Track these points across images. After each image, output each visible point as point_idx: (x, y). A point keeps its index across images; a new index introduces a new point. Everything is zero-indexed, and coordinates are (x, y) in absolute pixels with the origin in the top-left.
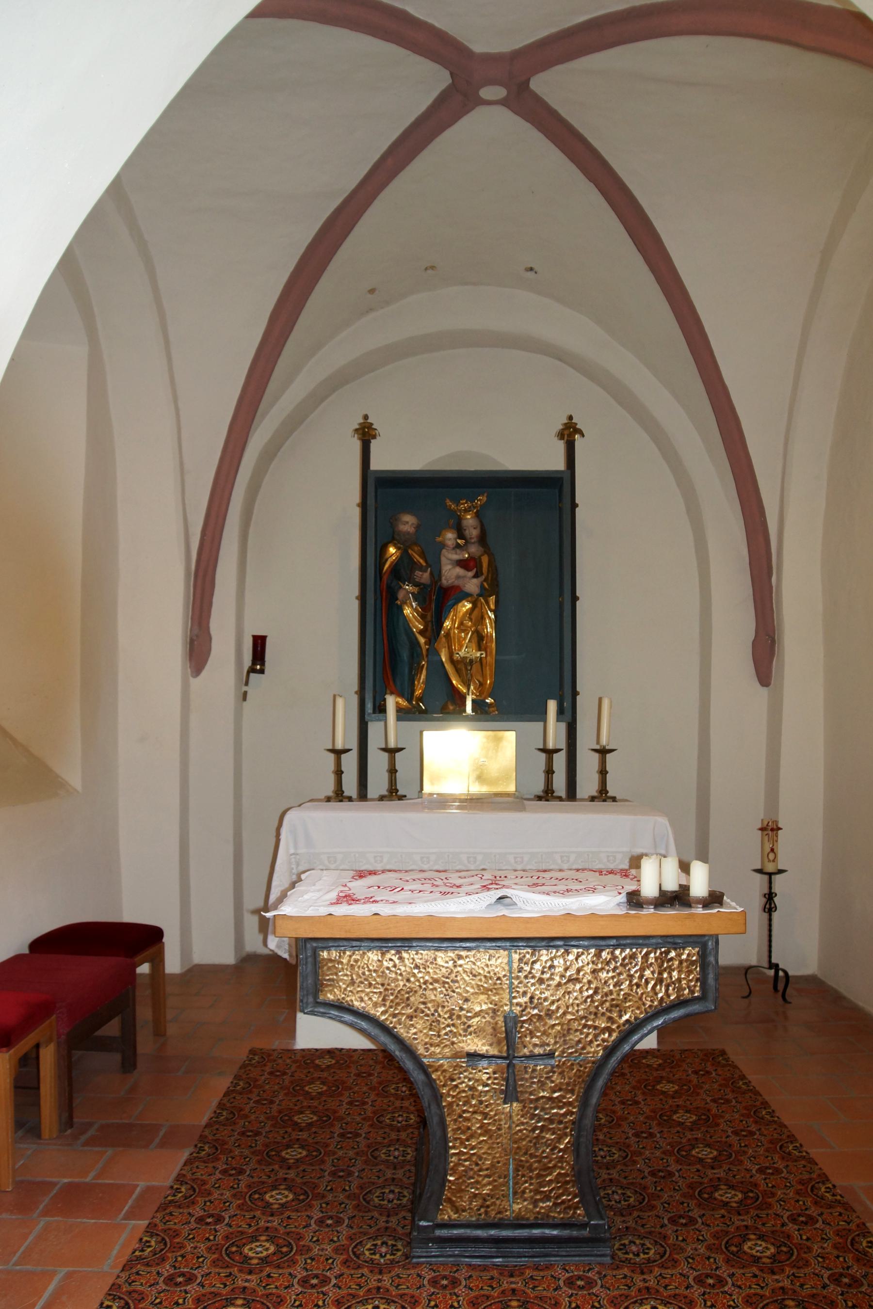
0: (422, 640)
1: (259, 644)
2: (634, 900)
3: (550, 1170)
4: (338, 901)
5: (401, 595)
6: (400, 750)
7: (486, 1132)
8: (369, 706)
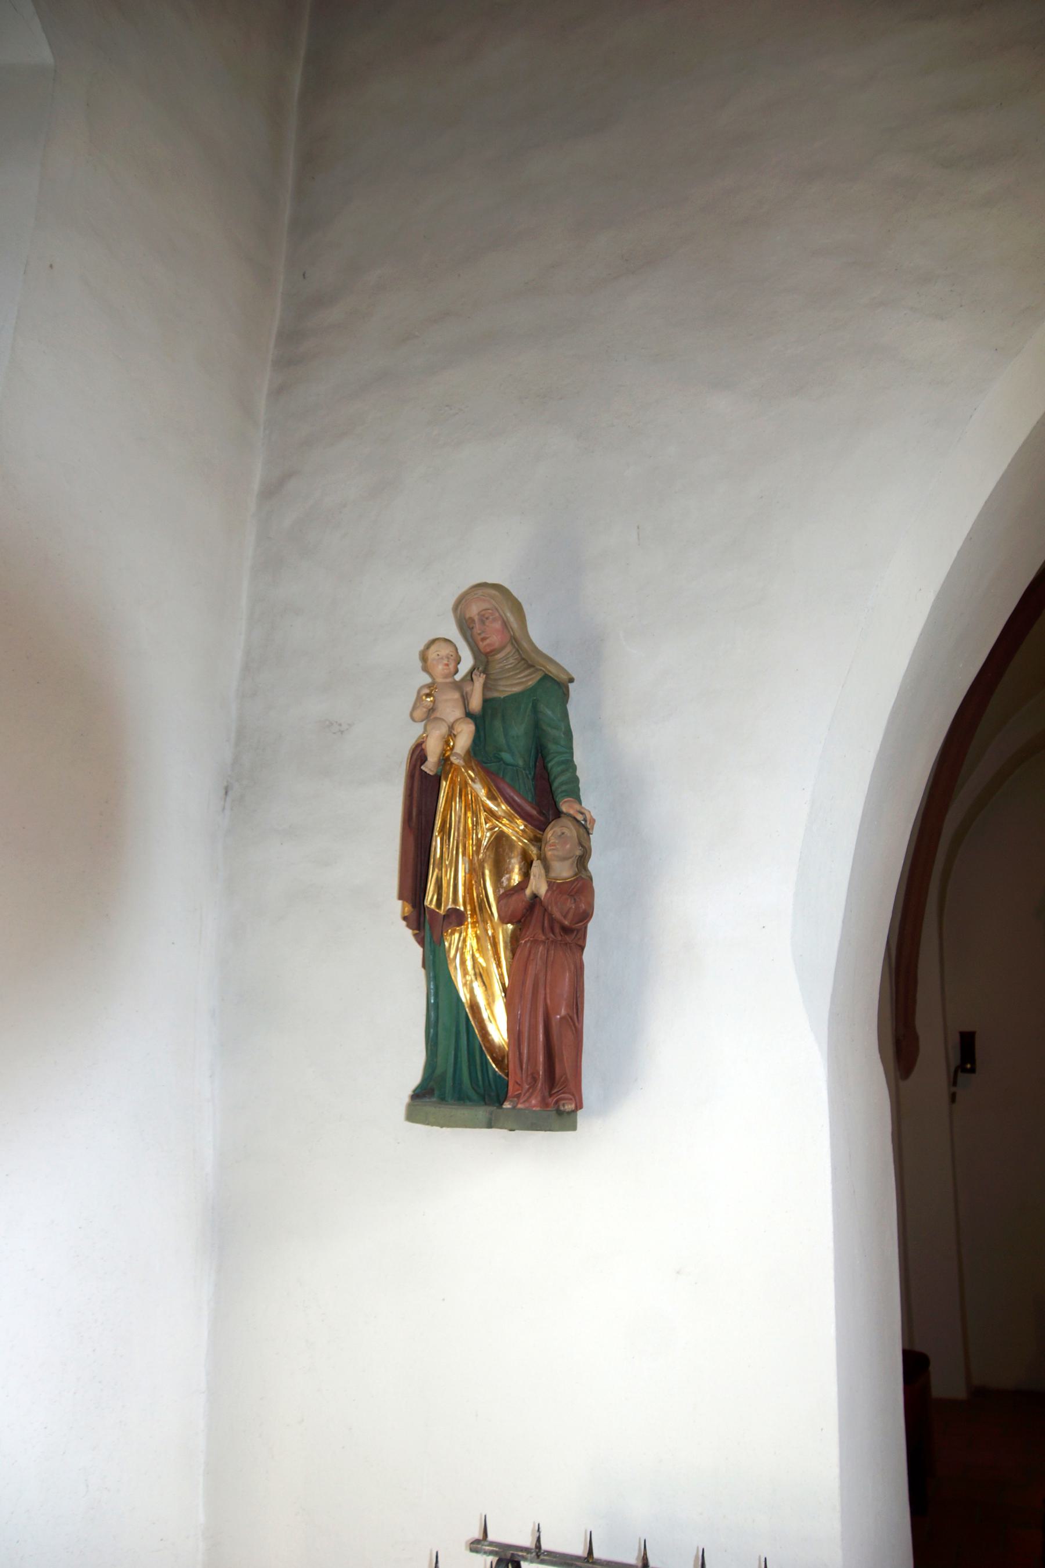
1: (967, 1042)
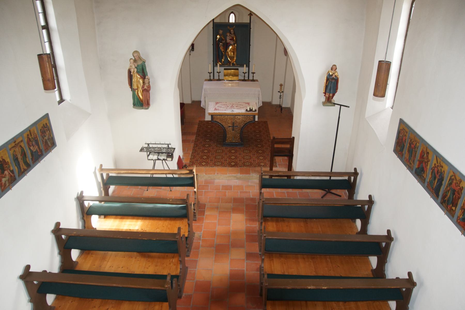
0: (223, 53)
2: (247, 110)
3: (237, 138)
5: (220, 45)
6: (220, 72)
7: (231, 134)
8: (215, 64)
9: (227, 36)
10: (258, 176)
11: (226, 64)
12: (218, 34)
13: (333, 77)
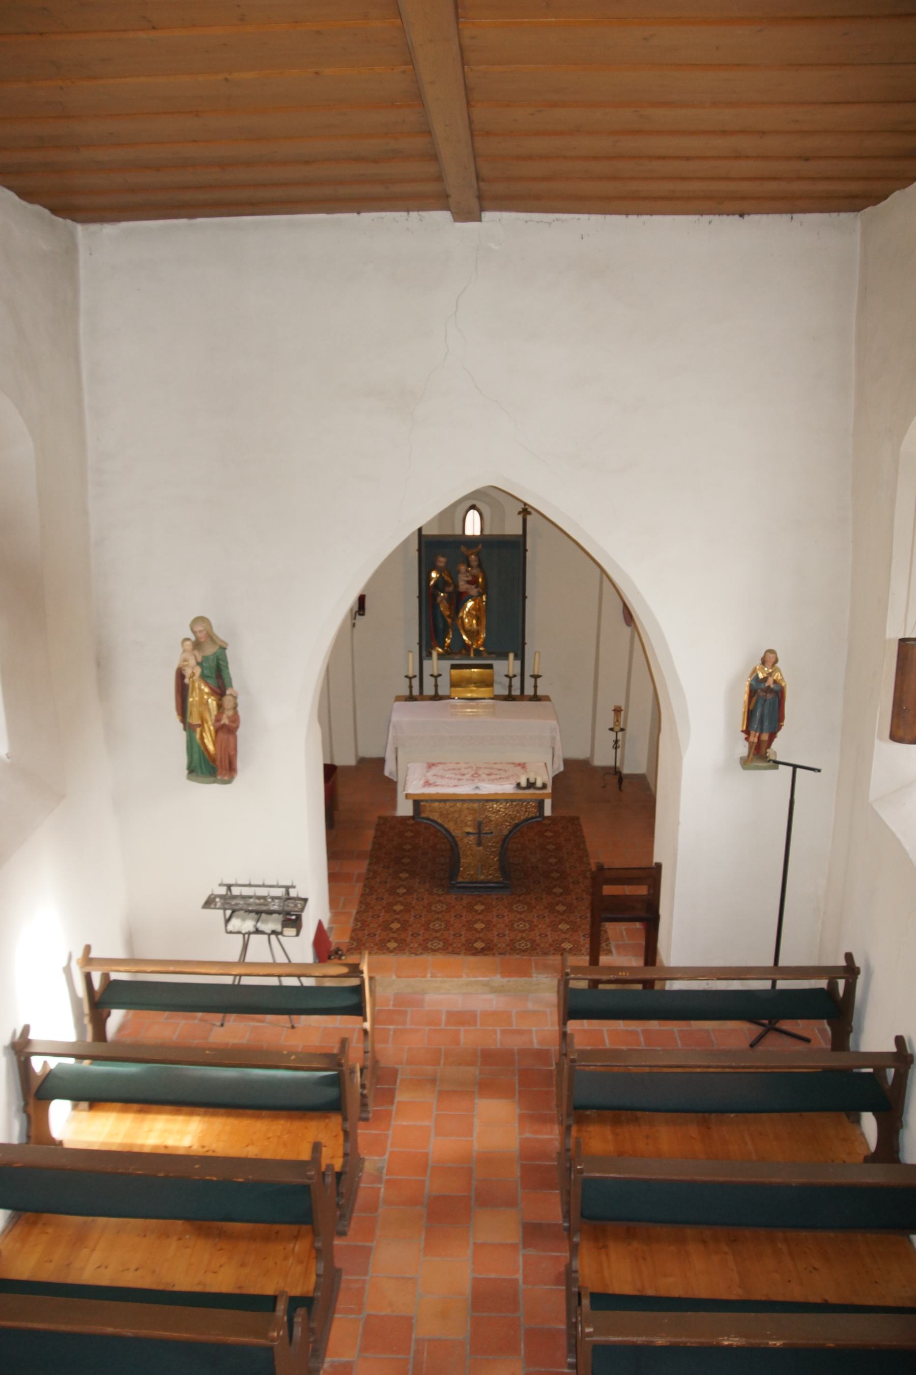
0: (449, 620)
3: (491, 866)
4: (424, 786)
5: (439, 599)
6: (440, 675)
8: (424, 653)
9: (458, 572)
10: (555, 982)
11: (457, 651)
12: (434, 568)
13: (767, 684)
